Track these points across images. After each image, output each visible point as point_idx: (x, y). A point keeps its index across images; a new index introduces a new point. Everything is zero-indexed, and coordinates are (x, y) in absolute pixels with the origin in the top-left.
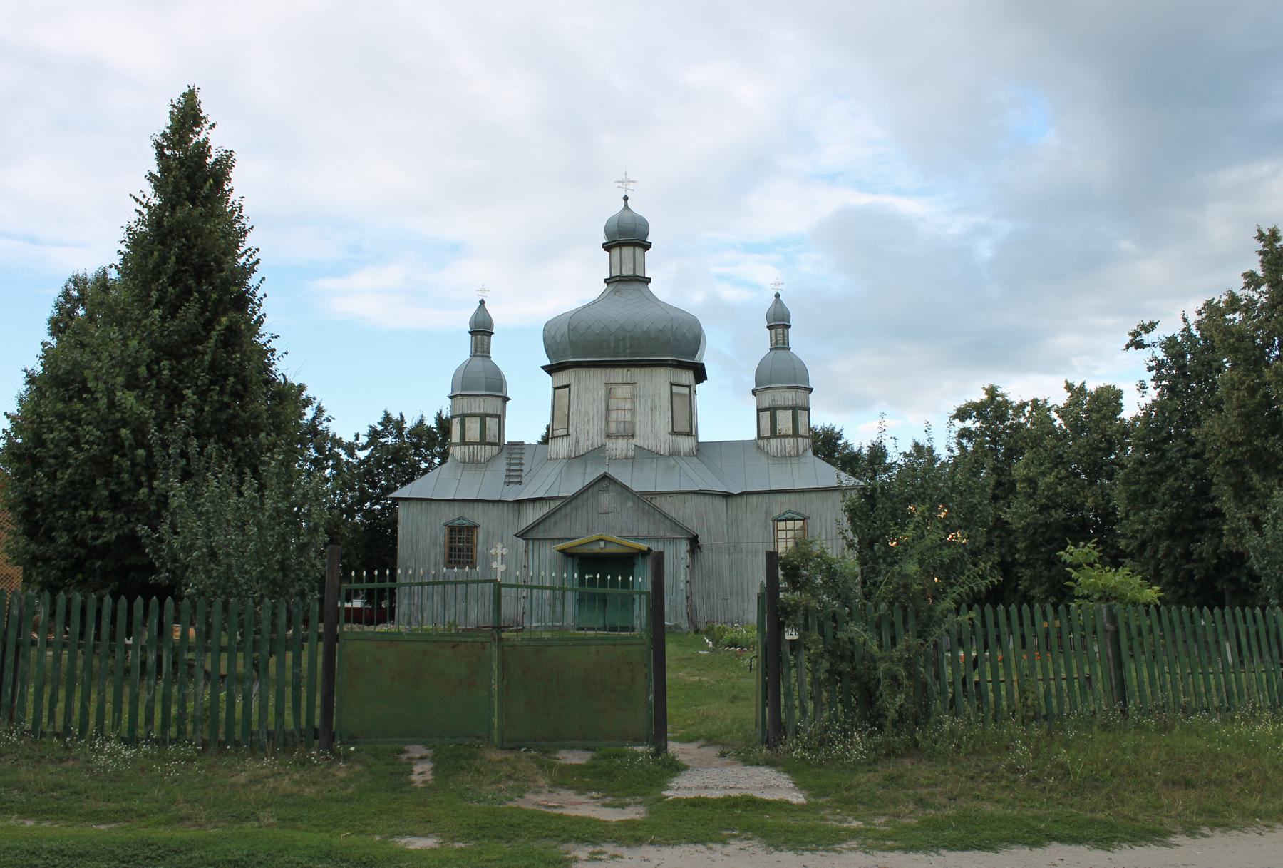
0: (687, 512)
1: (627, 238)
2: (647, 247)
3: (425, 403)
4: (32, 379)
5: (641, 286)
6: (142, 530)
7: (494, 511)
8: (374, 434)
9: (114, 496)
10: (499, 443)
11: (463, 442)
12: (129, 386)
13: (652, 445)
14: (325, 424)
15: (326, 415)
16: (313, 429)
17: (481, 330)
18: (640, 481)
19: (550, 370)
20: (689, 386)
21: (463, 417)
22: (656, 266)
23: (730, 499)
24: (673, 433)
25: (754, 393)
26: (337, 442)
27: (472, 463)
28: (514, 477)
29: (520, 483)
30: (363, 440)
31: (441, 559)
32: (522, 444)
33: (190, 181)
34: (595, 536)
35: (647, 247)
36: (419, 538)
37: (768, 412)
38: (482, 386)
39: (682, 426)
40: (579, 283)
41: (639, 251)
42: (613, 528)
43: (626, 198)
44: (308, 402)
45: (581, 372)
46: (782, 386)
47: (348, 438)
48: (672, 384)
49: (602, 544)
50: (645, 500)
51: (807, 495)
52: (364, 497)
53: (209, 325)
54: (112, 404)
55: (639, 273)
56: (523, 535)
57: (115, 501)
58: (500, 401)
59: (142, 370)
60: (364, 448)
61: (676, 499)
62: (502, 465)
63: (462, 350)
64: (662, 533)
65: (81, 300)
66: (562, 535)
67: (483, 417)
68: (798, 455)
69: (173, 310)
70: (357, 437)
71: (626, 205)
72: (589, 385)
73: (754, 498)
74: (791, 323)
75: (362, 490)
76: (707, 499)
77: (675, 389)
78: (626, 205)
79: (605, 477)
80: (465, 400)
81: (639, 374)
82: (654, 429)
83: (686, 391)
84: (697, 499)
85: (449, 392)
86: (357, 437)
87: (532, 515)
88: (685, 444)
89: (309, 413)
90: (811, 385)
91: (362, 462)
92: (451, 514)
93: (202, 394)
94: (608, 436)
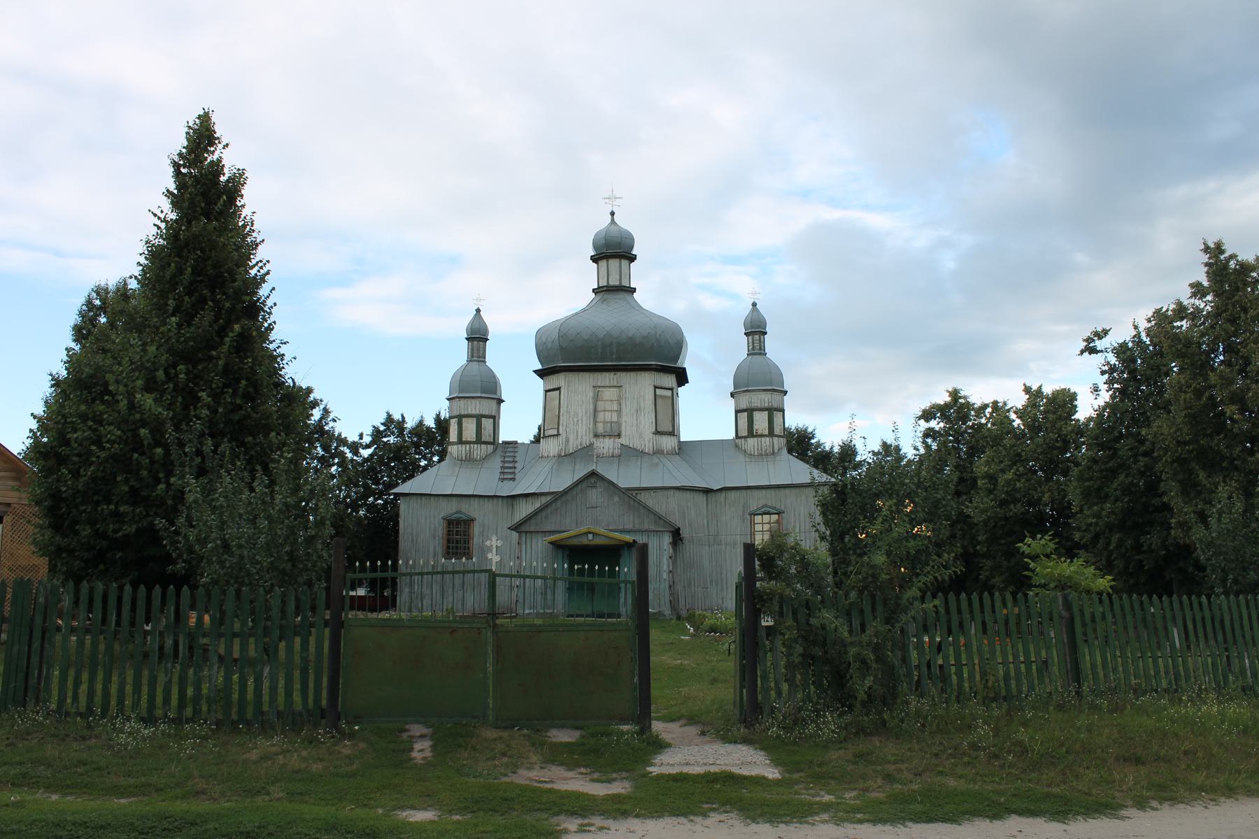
0: (670, 507)
1: (614, 250)
2: (632, 259)
3: (425, 404)
4: (57, 383)
5: (627, 296)
6: (160, 523)
7: (489, 506)
8: (377, 434)
9: (134, 492)
10: (494, 442)
11: (460, 441)
12: (148, 389)
13: (636, 443)
14: (331, 424)
15: (332, 416)
16: (319, 428)
17: (477, 337)
18: (626, 477)
19: (541, 373)
20: (672, 389)
21: (460, 418)
22: (640, 275)
23: (713, 497)
24: (657, 433)
25: (732, 395)
26: (343, 442)
27: (468, 460)
28: (508, 473)
29: (513, 479)
30: (367, 439)
31: (440, 551)
32: (516, 443)
33: (205, 194)
34: (583, 529)
35: (632, 259)
36: (419, 530)
37: (745, 413)
38: (478, 388)
39: (665, 426)
40: (569, 293)
41: (625, 262)
42: (600, 521)
43: (613, 214)
44: (315, 404)
45: (571, 375)
46: (758, 389)
47: (352, 438)
48: (656, 387)
49: (590, 536)
50: (631, 496)
51: (782, 491)
52: (368, 492)
53: (222, 332)
54: (132, 406)
55: (625, 283)
56: (516, 528)
57: (135, 496)
58: (494, 403)
59: (160, 374)
60: (368, 446)
61: (660, 493)
62: (496, 463)
63: (459, 355)
64: (646, 526)
65: (103, 309)
66: (553, 528)
67: (479, 418)
68: (773, 453)
69: (189, 318)
70: (361, 436)
71: (613, 220)
72: (578, 389)
73: (733, 494)
74: (767, 329)
75: (366, 486)
76: (688, 495)
77: (659, 392)
78: (613, 220)
79: (593, 474)
80: (462, 402)
81: (625, 378)
82: (638, 430)
83: (669, 393)
84: (678, 493)
85: (447, 395)
86: (361, 436)
87: (525, 509)
88: (668, 443)
89: (316, 414)
90: (786, 388)
91: (365, 460)
92: (449, 508)
93: (216, 396)
94: (596, 436)
